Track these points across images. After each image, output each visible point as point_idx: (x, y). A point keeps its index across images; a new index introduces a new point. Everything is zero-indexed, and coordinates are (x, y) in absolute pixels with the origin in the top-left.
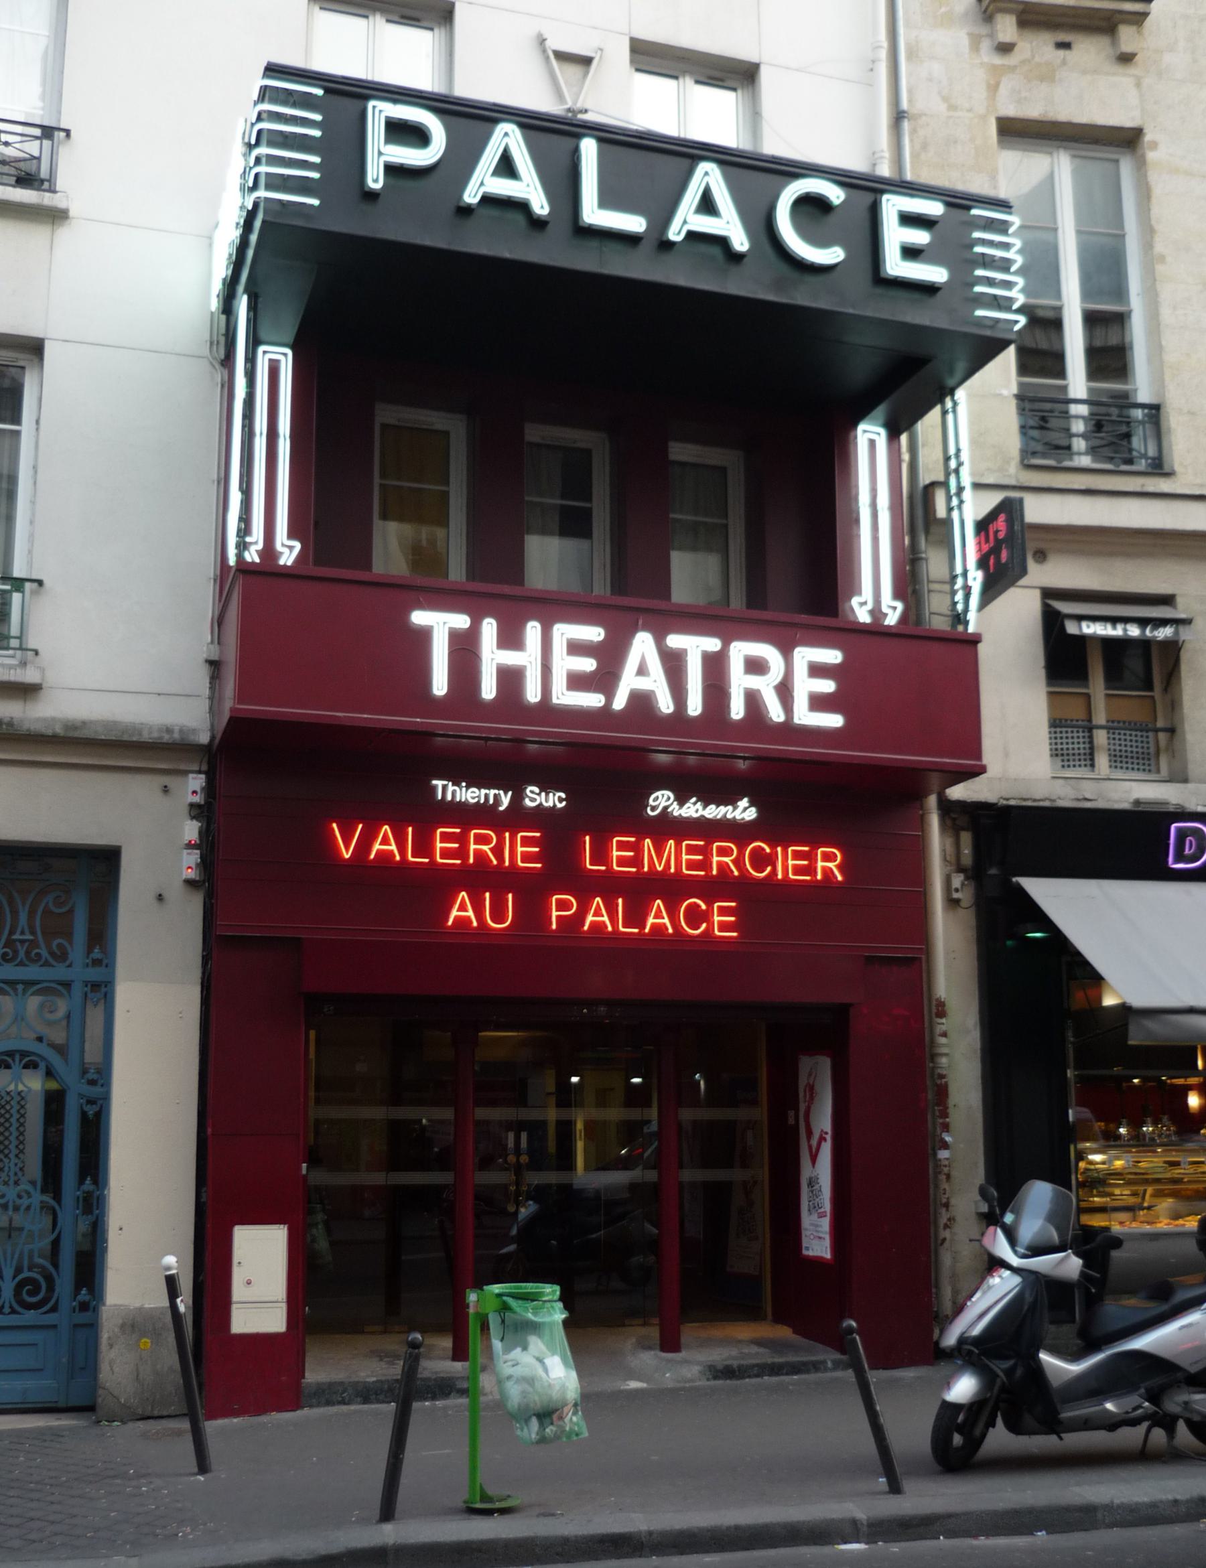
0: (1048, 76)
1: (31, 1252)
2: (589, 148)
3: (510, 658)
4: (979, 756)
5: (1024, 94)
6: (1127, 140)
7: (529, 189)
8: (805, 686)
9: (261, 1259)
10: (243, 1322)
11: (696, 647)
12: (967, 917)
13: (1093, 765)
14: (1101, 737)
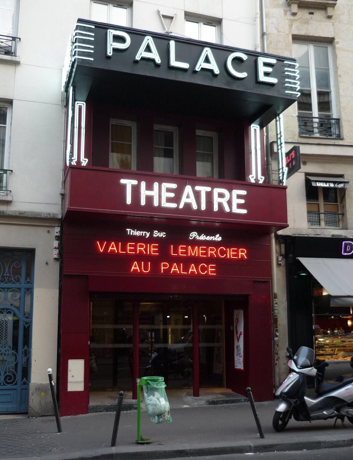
0: (307, 22)
1: (9, 367)
2: (172, 43)
3: (149, 193)
4: (287, 222)
5: (300, 28)
6: (330, 41)
7: (155, 55)
8: (236, 201)
9: (76, 369)
10: (71, 388)
11: (203, 190)
12: (283, 269)
13: (320, 225)
14: (322, 216)
